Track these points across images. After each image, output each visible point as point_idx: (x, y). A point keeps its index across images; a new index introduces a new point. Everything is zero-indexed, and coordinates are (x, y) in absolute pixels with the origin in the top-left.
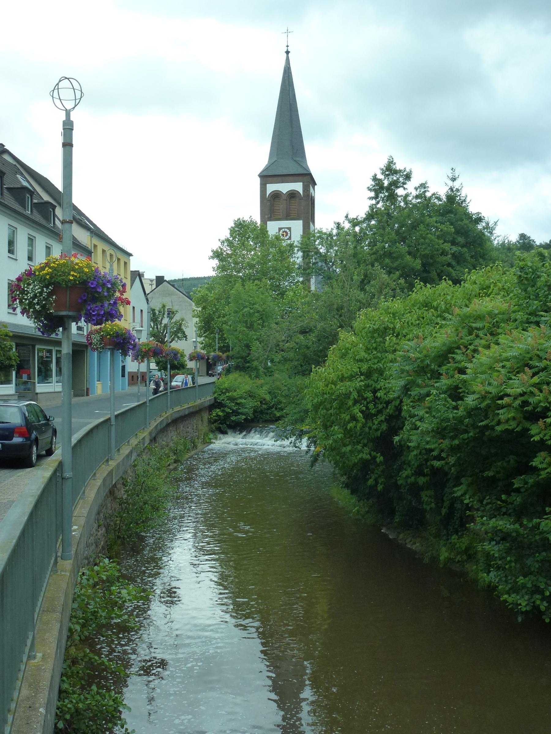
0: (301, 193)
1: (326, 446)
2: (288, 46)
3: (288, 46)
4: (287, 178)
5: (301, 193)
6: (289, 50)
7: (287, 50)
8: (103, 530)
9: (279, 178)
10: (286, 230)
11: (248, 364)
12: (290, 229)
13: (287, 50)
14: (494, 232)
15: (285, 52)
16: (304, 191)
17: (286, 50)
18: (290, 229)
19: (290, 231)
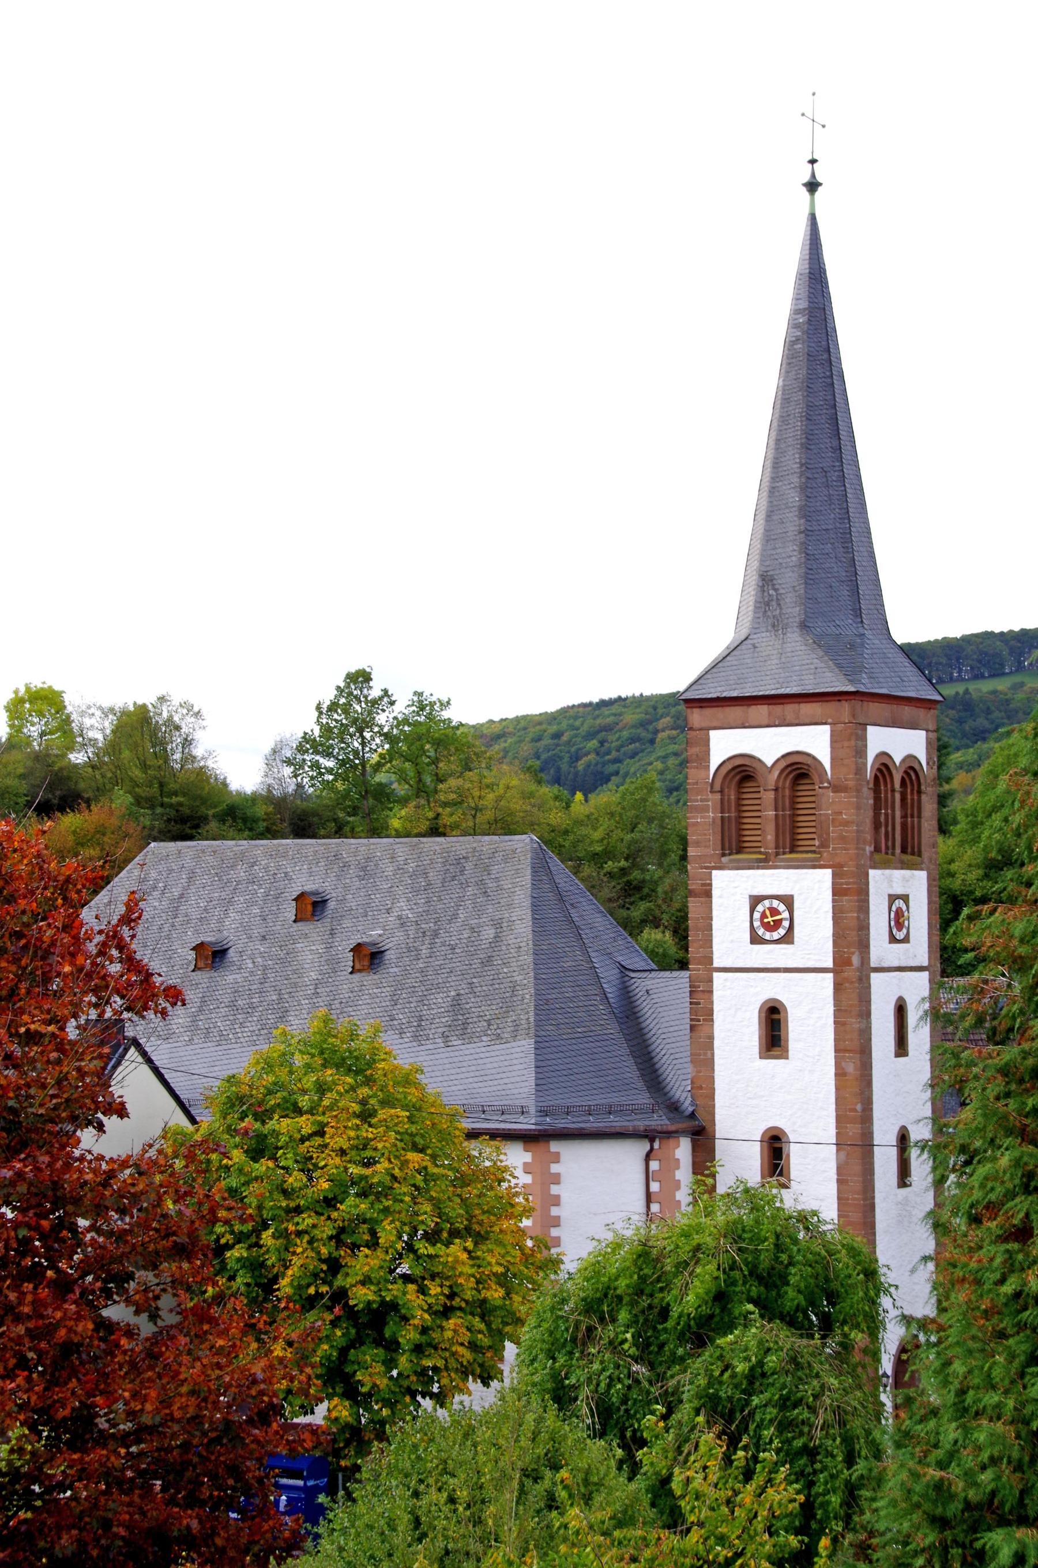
0: (827, 765)
1: (951, 731)
2: (812, 186)
3: (812, 186)
4: (790, 709)
5: (827, 765)
6: (819, 179)
7: (813, 175)
8: (880, 1336)
9: (762, 711)
10: (775, 903)
11: (571, 837)
12: (788, 901)
13: (813, 175)
14: (949, 802)
15: (805, 185)
16: (833, 760)
17: (806, 178)
18: (788, 901)
19: (790, 908)
